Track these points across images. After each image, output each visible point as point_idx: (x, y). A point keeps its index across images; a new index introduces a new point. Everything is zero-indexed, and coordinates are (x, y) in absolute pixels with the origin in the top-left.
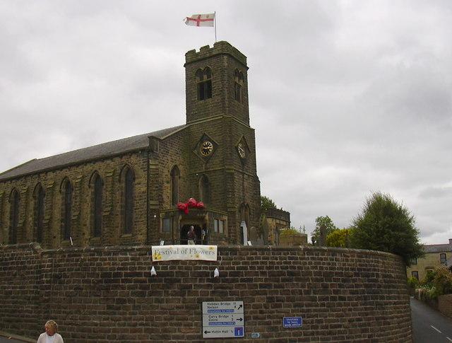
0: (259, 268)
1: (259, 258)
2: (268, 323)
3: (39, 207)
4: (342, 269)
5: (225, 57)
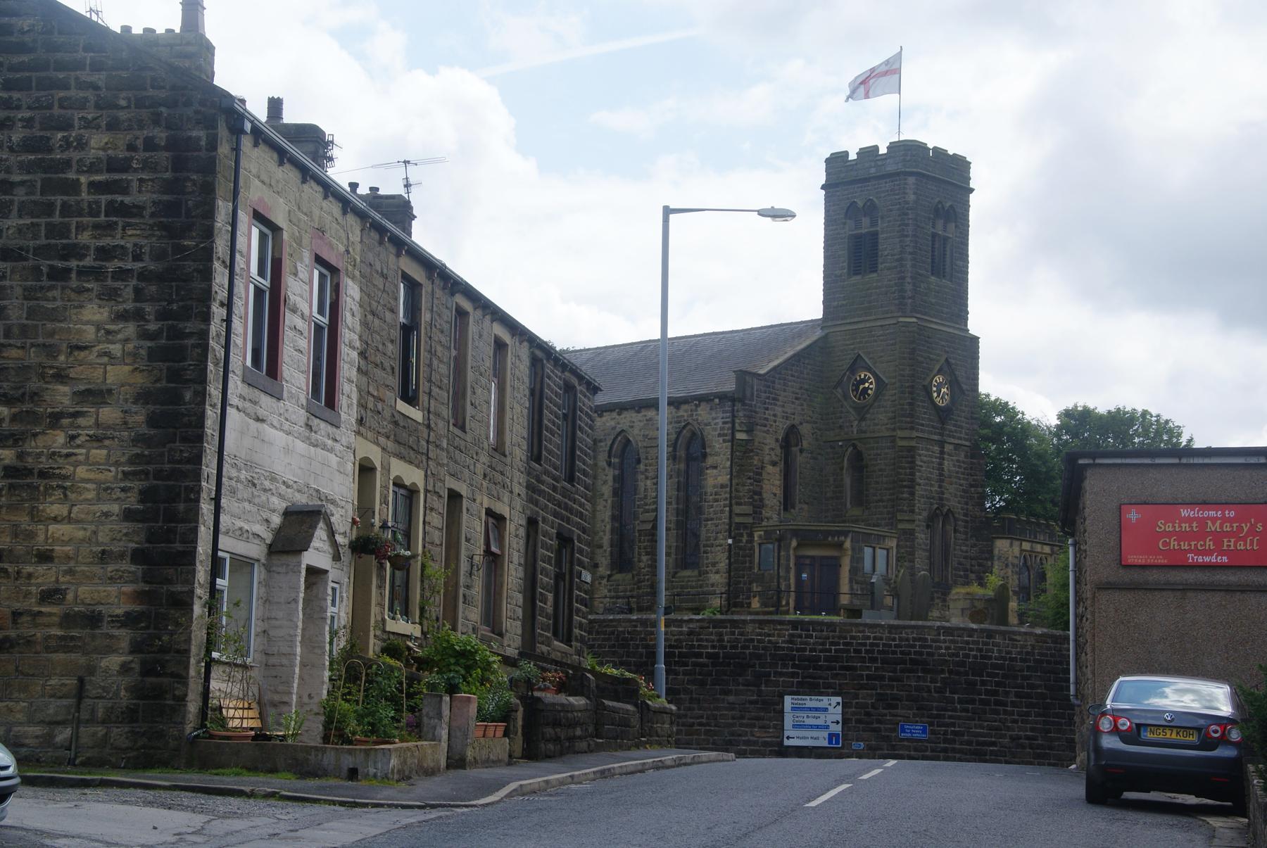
0: (867, 652)
1: (869, 638)
2: (874, 730)
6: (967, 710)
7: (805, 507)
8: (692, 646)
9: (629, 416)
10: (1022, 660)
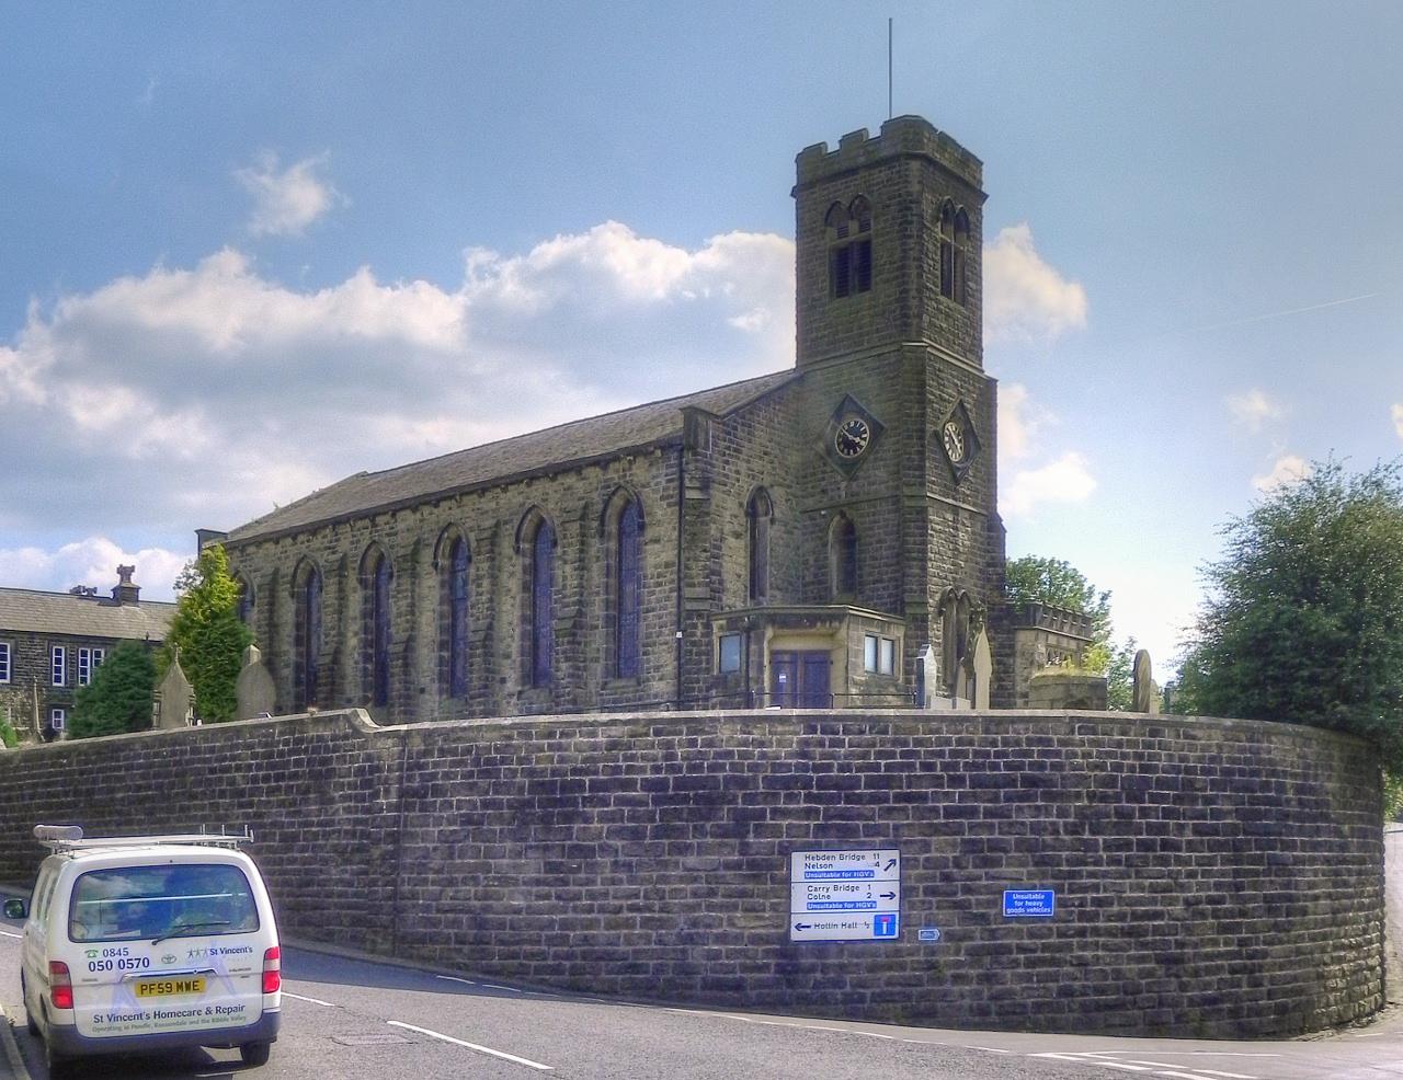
0: (946, 767)
1: (948, 742)
2: (957, 905)
3: (375, 611)
4: (1177, 770)
5: (915, 165)
6: (1118, 862)
7: (776, 593)
8: (617, 770)
9: (541, 487)
10: (1206, 771)
